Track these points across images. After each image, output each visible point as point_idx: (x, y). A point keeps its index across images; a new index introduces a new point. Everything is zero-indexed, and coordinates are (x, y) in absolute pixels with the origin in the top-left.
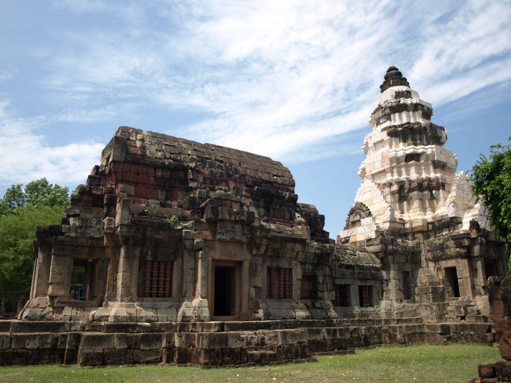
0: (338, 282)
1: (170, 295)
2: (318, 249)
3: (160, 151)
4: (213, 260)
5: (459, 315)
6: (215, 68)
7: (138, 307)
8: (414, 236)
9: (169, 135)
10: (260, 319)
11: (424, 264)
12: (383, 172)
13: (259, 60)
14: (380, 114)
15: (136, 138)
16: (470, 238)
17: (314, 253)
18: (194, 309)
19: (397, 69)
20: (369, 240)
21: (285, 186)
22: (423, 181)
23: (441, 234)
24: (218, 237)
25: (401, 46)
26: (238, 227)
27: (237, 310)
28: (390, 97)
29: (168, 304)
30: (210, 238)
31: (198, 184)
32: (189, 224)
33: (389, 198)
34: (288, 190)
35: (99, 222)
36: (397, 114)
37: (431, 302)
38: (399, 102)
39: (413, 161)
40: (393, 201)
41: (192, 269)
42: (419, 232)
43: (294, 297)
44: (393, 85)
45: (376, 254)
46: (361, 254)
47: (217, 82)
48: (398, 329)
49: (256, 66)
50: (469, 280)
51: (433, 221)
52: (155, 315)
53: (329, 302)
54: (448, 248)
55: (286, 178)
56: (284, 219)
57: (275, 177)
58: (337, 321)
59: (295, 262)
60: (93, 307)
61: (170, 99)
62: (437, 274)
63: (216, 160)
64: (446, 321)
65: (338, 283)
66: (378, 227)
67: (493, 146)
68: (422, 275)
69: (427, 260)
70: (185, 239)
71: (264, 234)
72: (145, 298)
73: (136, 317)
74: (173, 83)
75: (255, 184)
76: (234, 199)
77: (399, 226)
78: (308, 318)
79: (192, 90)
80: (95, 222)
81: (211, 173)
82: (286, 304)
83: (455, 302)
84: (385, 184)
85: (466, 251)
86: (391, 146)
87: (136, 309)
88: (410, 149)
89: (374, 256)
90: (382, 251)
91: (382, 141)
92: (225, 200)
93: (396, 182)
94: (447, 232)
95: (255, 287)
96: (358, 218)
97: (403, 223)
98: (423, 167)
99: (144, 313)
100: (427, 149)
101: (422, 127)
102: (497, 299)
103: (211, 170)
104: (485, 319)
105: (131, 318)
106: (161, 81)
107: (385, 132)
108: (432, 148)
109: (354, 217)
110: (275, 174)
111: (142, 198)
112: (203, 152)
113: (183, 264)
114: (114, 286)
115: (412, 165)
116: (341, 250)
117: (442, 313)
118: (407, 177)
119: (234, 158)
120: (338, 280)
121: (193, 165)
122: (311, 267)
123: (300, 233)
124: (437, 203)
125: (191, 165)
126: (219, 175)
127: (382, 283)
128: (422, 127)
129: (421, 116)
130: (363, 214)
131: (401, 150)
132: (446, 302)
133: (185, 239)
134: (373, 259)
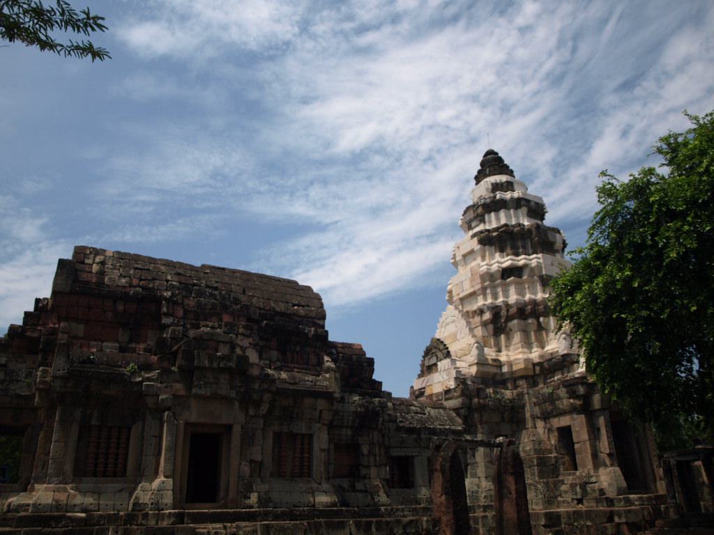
0: (395, 453)
1: (124, 474)
2: (360, 406)
3: (125, 277)
4: (187, 424)
5: (575, 497)
6: (323, 163)
7: (71, 491)
8: (515, 383)
9: (145, 255)
10: (251, 507)
11: (529, 424)
12: (473, 295)
13: (381, 151)
14: (471, 214)
15: (94, 260)
16: (586, 383)
17: (354, 412)
18: (152, 493)
19: (497, 154)
20: (448, 391)
21: (311, 320)
22: (526, 304)
23: (552, 379)
24: (194, 391)
25: (573, 123)
26: (224, 379)
27: (222, 494)
28: (485, 189)
29: (118, 486)
30: (182, 393)
31: (174, 320)
32: (154, 374)
33: (479, 332)
34: (315, 325)
35: (29, 375)
36: (493, 214)
37: (537, 478)
38: (495, 197)
39: (512, 278)
40: (486, 334)
42: (522, 377)
43: (314, 476)
44: (490, 175)
45: (456, 410)
46: (433, 412)
47: (325, 182)
48: (480, 520)
49: (377, 159)
50: (588, 443)
51: (541, 360)
52: (96, 502)
53: (377, 482)
54: (559, 398)
55: (313, 309)
56: (307, 364)
57: (296, 307)
58: (386, 510)
59: (317, 424)
60: (18, 491)
61: (264, 208)
62: (549, 437)
63: (207, 286)
64: (558, 507)
66: (458, 372)
67: (572, 252)
68: (526, 440)
69: (534, 418)
70: (146, 395)
71: (265, 386)
72: (85, 479)
73: (67, 505)
74: (266, 187)
75: (264, 317)
76: (222, 340)
77: (494, 370)
78: (334, 504)
79: (292, 194)
80: (23, 375)
81: (199, 304)
82: (301, 485)
83: (571, 477)
84: (475, 312)
85: (581, 402)
86: (483, 258)
87: (67, 494)
88: (507, 261)
89: (454, 415)
90: (463, 406)
91: (472, 252)
92: (208, 340)
93: (488, 307)
94: (559, 376)
95: (251, 461)
96: (433, 360)
97: (498, 364)
98: (527, 286)
99: (79, 500)
100: (531, 260)
101: (526, 229)
102: (436, 470)
103: (198, 301)
104: (610, 502)
105: (57, 506)
106: (251, 184)
107: (476, 239)
108: (539, 258)
109: (429, 359)
110: (297, 302)
111: (95, 340)
112: (190, 276)
114: (45, 462)
115: (510, 283)
116: (402, 407)
117: (552, 495)
118: (505, 299)
119: (236, 283)
121: (168, 294)
122: (349, 432)
123: (325, 383)
124: (547, 336)
125: (165, 294)
126: (208, 307)
128: (526, 229)
129: (525, 215)
130: (439, 354)
131: (495, 263)
132: (560, 478)
133: (146, 395)
134: (451, 419)
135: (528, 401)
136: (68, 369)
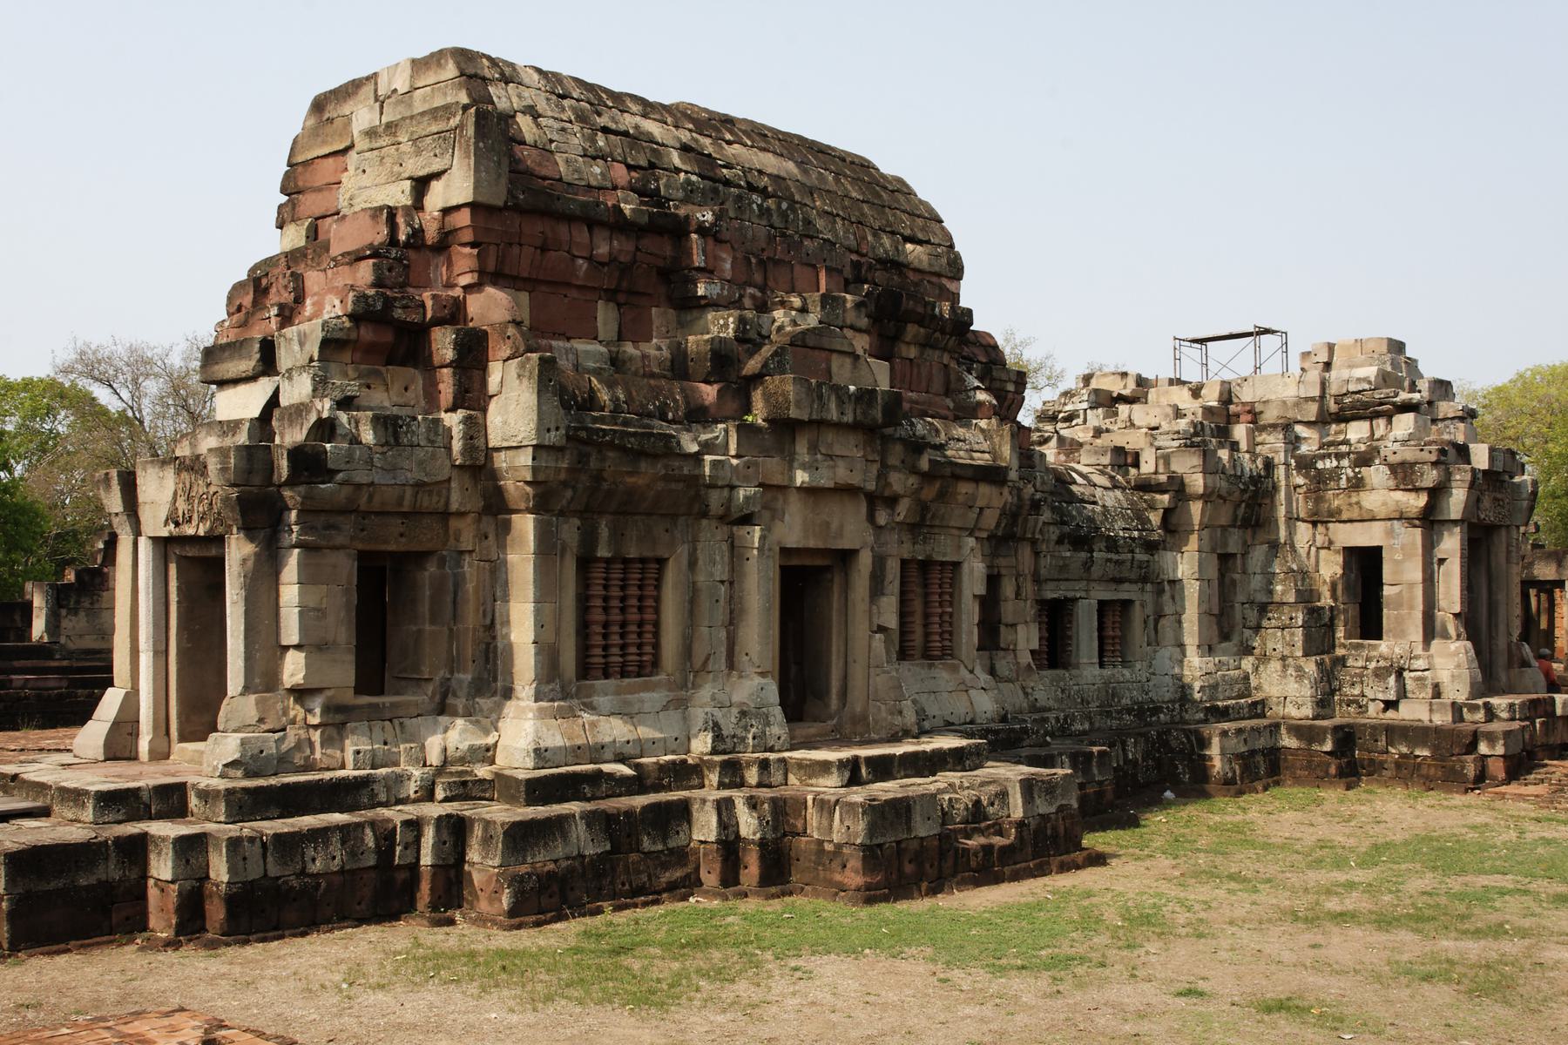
1: (656, 664)
27: (834, 702)
41: (722, 582)
113: (693, 564)
127: (1160, 592)
135: (1283, 483)
136: (568, 427)
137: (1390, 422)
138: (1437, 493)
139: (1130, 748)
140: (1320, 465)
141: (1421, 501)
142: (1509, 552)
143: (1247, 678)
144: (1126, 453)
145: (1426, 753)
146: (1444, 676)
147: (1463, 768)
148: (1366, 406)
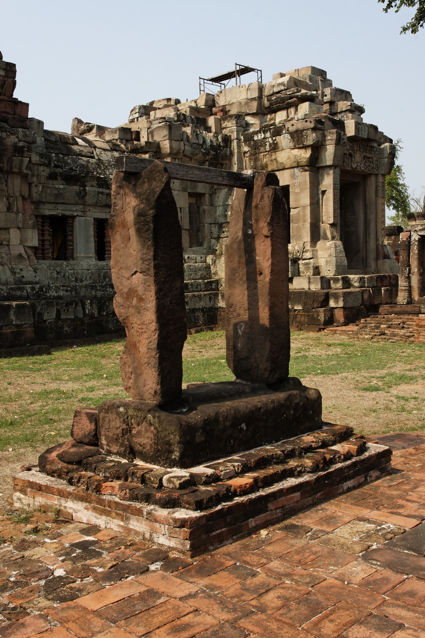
0: (48, 211)
65: (47, 212)
120: (47, 206)
137: (296, 110)
138: (317, 148)
139: (88, 306)
140: (256, 138)
141: (306, 154)
142: (377, 191)
143: (208, 267)
144: (132, 132)
145: (300, 308)
146: (322, 262)
147: (318, 315)
148: (283, 100)
